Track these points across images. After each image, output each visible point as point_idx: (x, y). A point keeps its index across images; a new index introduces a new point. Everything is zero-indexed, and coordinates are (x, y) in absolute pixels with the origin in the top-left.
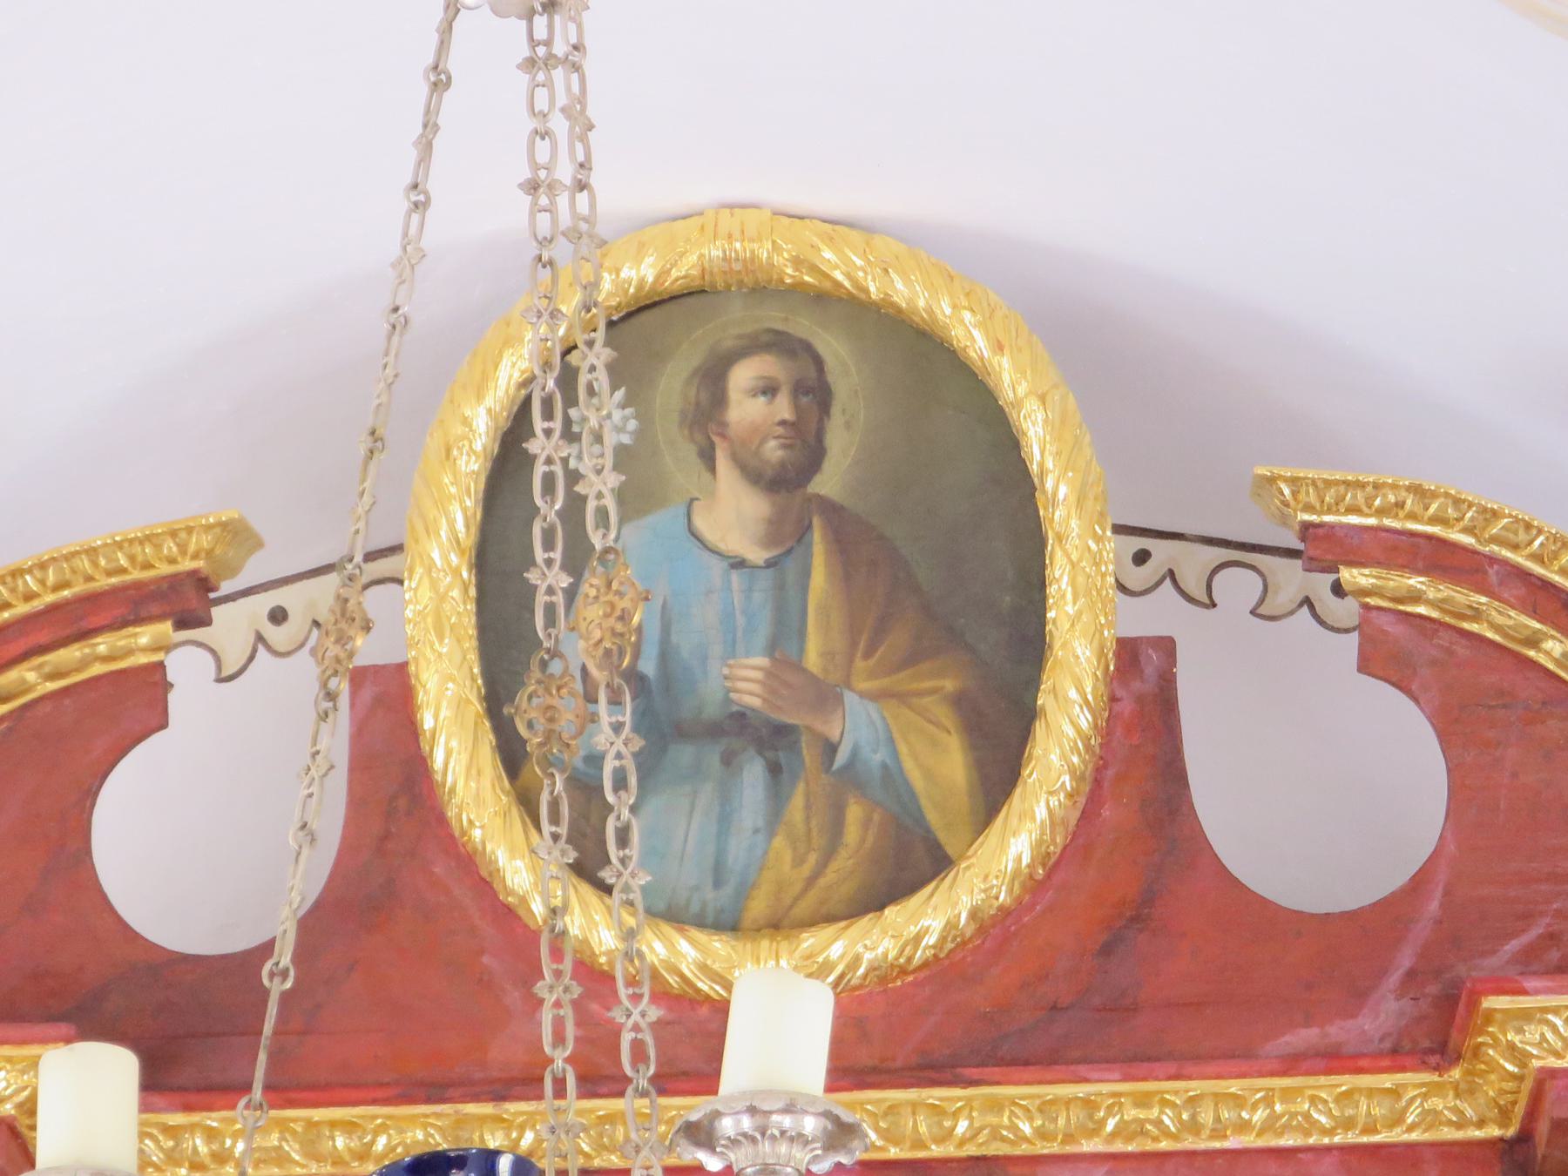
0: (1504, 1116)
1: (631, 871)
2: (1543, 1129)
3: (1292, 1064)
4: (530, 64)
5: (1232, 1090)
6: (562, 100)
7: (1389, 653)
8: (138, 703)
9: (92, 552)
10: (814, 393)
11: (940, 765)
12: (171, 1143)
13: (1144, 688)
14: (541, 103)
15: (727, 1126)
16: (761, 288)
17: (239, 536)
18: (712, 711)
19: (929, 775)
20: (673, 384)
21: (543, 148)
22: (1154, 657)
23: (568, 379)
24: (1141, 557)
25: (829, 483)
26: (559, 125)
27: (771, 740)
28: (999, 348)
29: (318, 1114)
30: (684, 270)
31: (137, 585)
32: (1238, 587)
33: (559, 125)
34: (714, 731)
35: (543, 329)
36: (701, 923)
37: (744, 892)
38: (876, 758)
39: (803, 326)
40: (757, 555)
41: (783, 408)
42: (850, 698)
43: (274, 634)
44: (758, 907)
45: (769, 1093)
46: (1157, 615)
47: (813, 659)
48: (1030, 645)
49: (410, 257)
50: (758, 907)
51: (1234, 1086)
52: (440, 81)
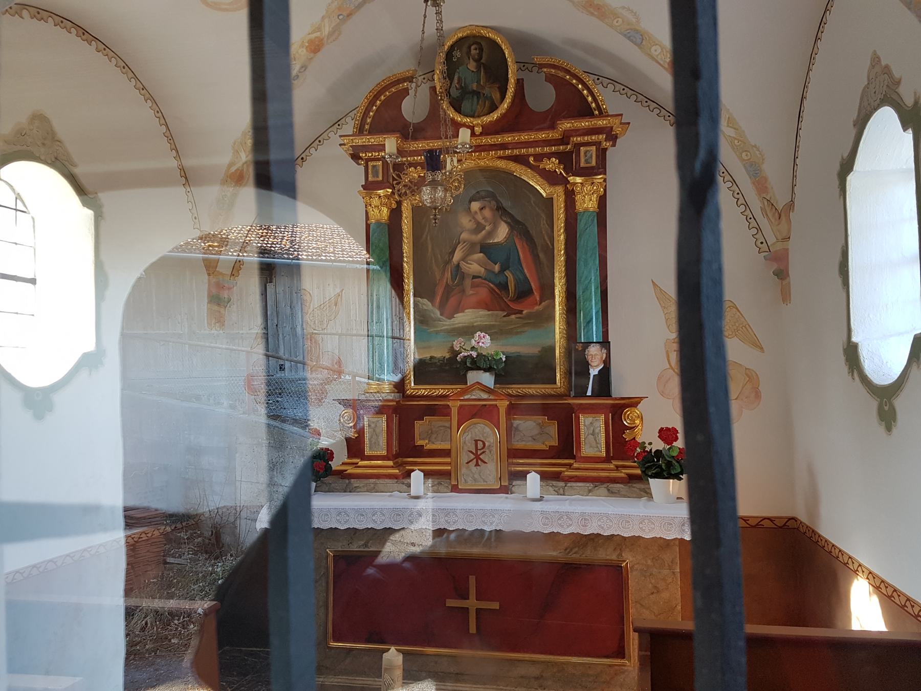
1: (647, 530)
7: (550, 79)
8: (406, 92)
10: (481, 50)
11: (496, 96)
12: (620, 20)
13: (520, 83)
16: (474, 36)
20: (465, 49)
25: (483, 61)
27: (477, 93)
30: (465, 34)
35: (497, 268)
48: (507, 80)
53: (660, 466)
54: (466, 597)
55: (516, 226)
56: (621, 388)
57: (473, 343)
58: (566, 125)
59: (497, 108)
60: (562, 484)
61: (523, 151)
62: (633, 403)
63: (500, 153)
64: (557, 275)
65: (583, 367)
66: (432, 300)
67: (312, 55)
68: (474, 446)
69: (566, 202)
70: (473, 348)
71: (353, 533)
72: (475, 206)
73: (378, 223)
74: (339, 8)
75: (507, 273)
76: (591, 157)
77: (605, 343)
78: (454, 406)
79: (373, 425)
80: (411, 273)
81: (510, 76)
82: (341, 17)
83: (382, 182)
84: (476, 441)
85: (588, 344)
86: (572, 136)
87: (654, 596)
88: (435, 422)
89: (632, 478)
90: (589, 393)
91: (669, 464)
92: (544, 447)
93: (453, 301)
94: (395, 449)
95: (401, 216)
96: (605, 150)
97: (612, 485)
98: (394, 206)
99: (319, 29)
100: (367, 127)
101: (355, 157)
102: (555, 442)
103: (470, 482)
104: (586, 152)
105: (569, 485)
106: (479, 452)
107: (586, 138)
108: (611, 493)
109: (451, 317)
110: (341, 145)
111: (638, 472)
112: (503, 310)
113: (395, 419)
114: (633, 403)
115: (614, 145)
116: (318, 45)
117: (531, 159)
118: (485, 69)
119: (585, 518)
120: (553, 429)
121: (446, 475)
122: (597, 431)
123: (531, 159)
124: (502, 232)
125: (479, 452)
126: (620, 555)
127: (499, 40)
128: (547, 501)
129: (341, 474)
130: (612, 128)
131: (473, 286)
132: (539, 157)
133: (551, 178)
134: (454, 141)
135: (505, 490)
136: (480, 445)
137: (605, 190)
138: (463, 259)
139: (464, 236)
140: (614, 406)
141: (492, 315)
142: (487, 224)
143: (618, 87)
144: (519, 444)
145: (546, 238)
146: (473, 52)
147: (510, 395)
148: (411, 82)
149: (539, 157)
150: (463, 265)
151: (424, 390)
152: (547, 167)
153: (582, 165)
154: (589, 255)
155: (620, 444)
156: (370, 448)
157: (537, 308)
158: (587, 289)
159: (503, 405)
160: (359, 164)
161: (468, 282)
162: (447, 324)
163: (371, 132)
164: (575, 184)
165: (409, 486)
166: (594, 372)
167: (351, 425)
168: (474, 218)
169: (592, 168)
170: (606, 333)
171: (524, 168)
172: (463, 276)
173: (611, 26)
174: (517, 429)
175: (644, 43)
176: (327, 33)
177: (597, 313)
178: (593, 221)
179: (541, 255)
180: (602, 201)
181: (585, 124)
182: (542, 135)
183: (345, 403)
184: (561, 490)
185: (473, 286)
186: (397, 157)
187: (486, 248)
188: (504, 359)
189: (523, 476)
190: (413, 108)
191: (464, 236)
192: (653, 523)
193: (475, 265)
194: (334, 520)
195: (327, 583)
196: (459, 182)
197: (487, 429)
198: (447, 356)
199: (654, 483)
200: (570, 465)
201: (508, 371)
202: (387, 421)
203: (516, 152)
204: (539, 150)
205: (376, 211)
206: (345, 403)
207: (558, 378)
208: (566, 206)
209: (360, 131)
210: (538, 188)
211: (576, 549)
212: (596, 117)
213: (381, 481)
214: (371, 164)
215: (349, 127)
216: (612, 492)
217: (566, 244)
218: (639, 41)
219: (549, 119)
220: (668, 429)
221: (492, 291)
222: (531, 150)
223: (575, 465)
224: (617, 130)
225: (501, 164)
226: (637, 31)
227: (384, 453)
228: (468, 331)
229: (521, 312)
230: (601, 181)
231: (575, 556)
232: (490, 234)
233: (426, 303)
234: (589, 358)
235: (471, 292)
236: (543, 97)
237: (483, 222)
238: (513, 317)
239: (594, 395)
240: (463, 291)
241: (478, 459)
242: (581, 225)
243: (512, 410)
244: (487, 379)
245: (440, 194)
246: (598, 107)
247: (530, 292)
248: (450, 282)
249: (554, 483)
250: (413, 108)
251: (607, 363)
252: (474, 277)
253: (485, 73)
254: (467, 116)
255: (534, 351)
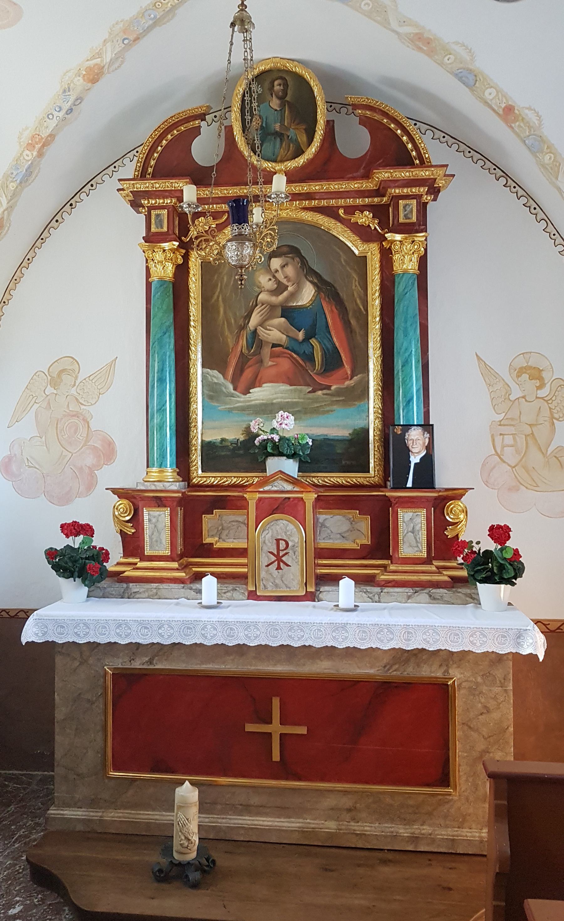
0: (376, 186)
2: (381, 188)
3: (349, 179)
4: (244, 40)
5: (352, 322)
6: (249, 47)
7: (364, 121)
8: (197, 131)
9: (189, 110)
10: (286, 85)
11: (302, 138)
14: (246, 47)
15: (273, 196)
16: (279, 70)
17: (209, 107)
18: (273, 131)
19: (301, 140)
20: (267, 84)
21: (246, 53)
22: (331, 123)
23: (250, 88)
24: (331, 106)
25: (288, 98)
26: (248, 50)
27: (280, 135)
28: (311, 78)
29: (222, 188)
30: (268, 67)
31: (196, 115)
32: (344, 110)
33: (248, 50)
34: (273, 134)
35: (301, 335)
36: (271, 161)
37: (277, 157)
38: (294, 138)
39: (284, 75)
40: (278, 109)
41: (282, 87)
42: (291, 129)
43: (215, 119)
44: (279, 159)
45: (278, 192)
46: (333, 116)
47: (286, 124)
48: (315, 121)
49: (228, 70)
50: (279, 159)
51: (341, 182)
52: (232, 44)
53: (492, 570)
54: (268, 721)
55: (324, 287)
56: (444, 479)
57: (275, 424)
58: (383, 174)
59: (303, 152)
60: (377, 589)
61: (333, 202)
62: (456, 494)
63: (306, 203)
64: (371, 344)
65: (404, 451)
66: (223, 373)
67: (90, 85)
68: (275, 547)
69: (381, 261)
70: (273, 430)
71: (135, 648)
72: (276, 263)
73: (162, 281)
74: (125, 31)
75: (313, 341)
76: (411, 211)
77: (427, 427)
78: (252, 498)
79: (154, 520)
80: (200, 340)
81: (319, 117)
82: (126, 42)
83: (167, 233)
84: (278, 540)
85: (407, 427)
86: (390, 187)
87: (484, 716)
88: (228, 516)
89: (456, 581)
90: (409, 484)
91: (501, 567)
92: (355, 546)
93: (248, 373)
94: (179, 548)
95: (189, 273)
96: (425, 204)
97: (434, 591)
98: (180, 261)
99: (99, 55)
100: (150, 170)
101: (135, 205)
102: (367, 541)
103: (270, 589)
104: (405, 206)
105: (386, 590)
106: (281, 553)
107: (405, 190)
108: (433, 599)
109: (246, 392)
110: (119, 190)
111: (464, 573)
112: (308, 385)
113: (180, 512)
114: (456, 494)
115: (435, 200)
116: (97, 74)
117: (341, 212)
118: (290, 108)
119: (408, 630)
120: (364, 525)
121: (242, 578)
122: (418, 528)
123: (341, 212)
124: (307, 295)
125: (281, 553)
126: (447, 671)
127: (307, 76)
128: (363, 610)
129: (117, 576)
130: (435, 179)
131: (273, 356)
132: (351, 210)
133: (365, 234)
134: (266, 189)
135: (311, 597)
136: (282, 545)
137: (426, 250)
138: (262, 324)
139: (263, 297)
140: (436, 498)
141: (295, 390)
142: (289, 284)
143: (438, 134)
144: (325, 543)
145: (358, 301)
146: (277, 88)
147: (315, 485)
148: (204, 119)
149: (351, 210)
150: (261, 331)
151: (214, 478)
152: (360, 221)
153: (401, 220)
154: (409, 324)
155: (444, 544)
156: (151, 547)
157: (347, 383)
158: (406, 363)
159: (310, 497)
160: (139, 212)
161: (266, 351)
162: (241, 399)
163: (154, 176)
164: (392, 242)
165: (199, 591)
166: (415, 459)
167: (128, 518)
168: (274, 277)
169: (413, 224)
170: (427, 414)
171: (333, 221)
172: (261, 344)
173: (441, 64)
174: (323, 525)
175: (477, 85)
176: (108, 60)
177: (418, 391)
178: (413, 284)
179: (353, 322)
180: (423, 262)
181: (405, 174)
182: (355, 185)
183: (121, 493)
184: (376, 598)
185: (273, 356)
186: (197, 207)
187: (287, 312)
188: (311, 444)
189: (334, 580)
190: (205, 149)
191: (263, 297)
192: (485, 636)
193: (275, 332)
194: (113, 633)
195: (106, 705)
196: (273, 238)
197: (291, 527)
198: (242, 438)
199: (481, 587)
200: (385, 567)
201: (316, 457)
202: (171, 515)
203: (324, 203)
204: (350, 202)
205: (160, 267)
206: (121, 493)
207: (372, 465)
208: (381, 267)
209: (142, 175)
210: (350, 244)
211: (397, 666)
212: (417, 166)
213: (165, 586)
214: (153, 213)
215: (129, 169)
216: (434, 599)
217: (382, 309)
218: (472, 83)
219: (363, 167)
220: (499, 527)
221: (295, 362)
222: (341, 202)
223: (392, 567)
224: (440, 183)
225: (308, 216)
226: (470, 71)
227: (168, 553)
228: (268, 410)
229: (329, 388)
230: (424, 239)
231: (396, 673)
232: (293, 296)
233: (216, 376)
234: (410, 444)
235: (270, 363)
236: (356, 141)
237: (284, 281)
238: (320, 393)
239: (414, 488)
240: (261, 361)
241: (279, 560)
242: (399, 289)
243: (322, 503)
244: (291, 467)
245: (248, 250)
246: (420, 156)
247: (339, 364)
248: (245, 351)
249: (369, 588)
250: (205, 149)
251: (430, 448)
252: (274, 346)
253: (290, 111)
254: (268, 160)
255: (344, 433)
